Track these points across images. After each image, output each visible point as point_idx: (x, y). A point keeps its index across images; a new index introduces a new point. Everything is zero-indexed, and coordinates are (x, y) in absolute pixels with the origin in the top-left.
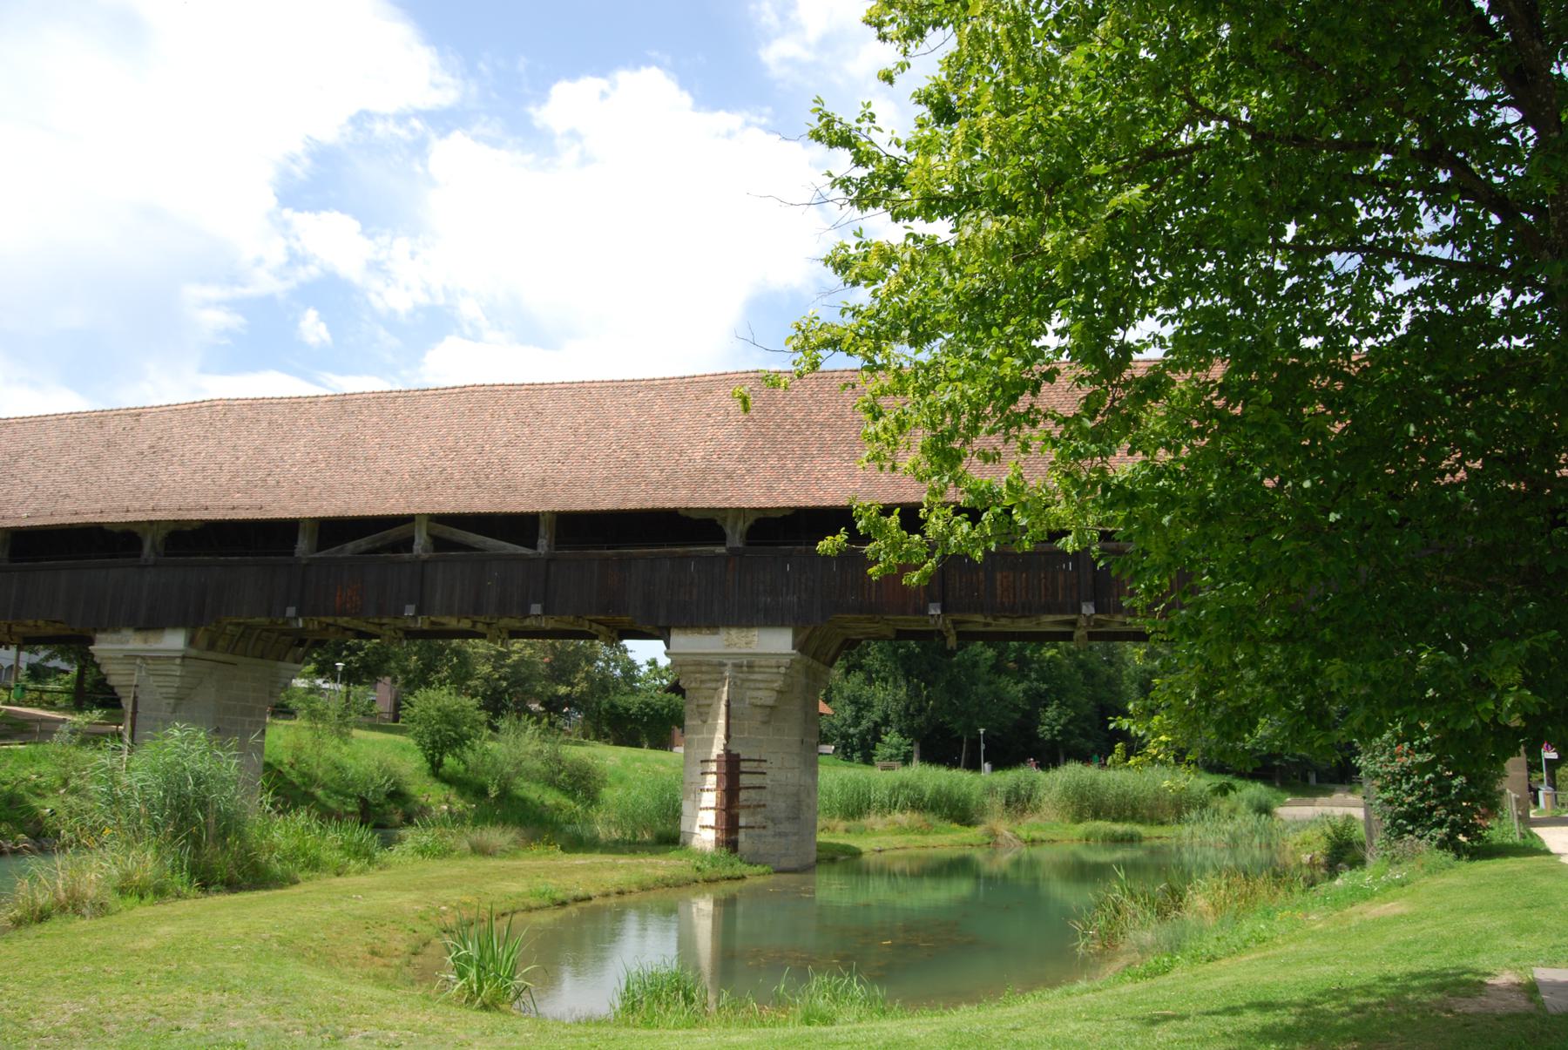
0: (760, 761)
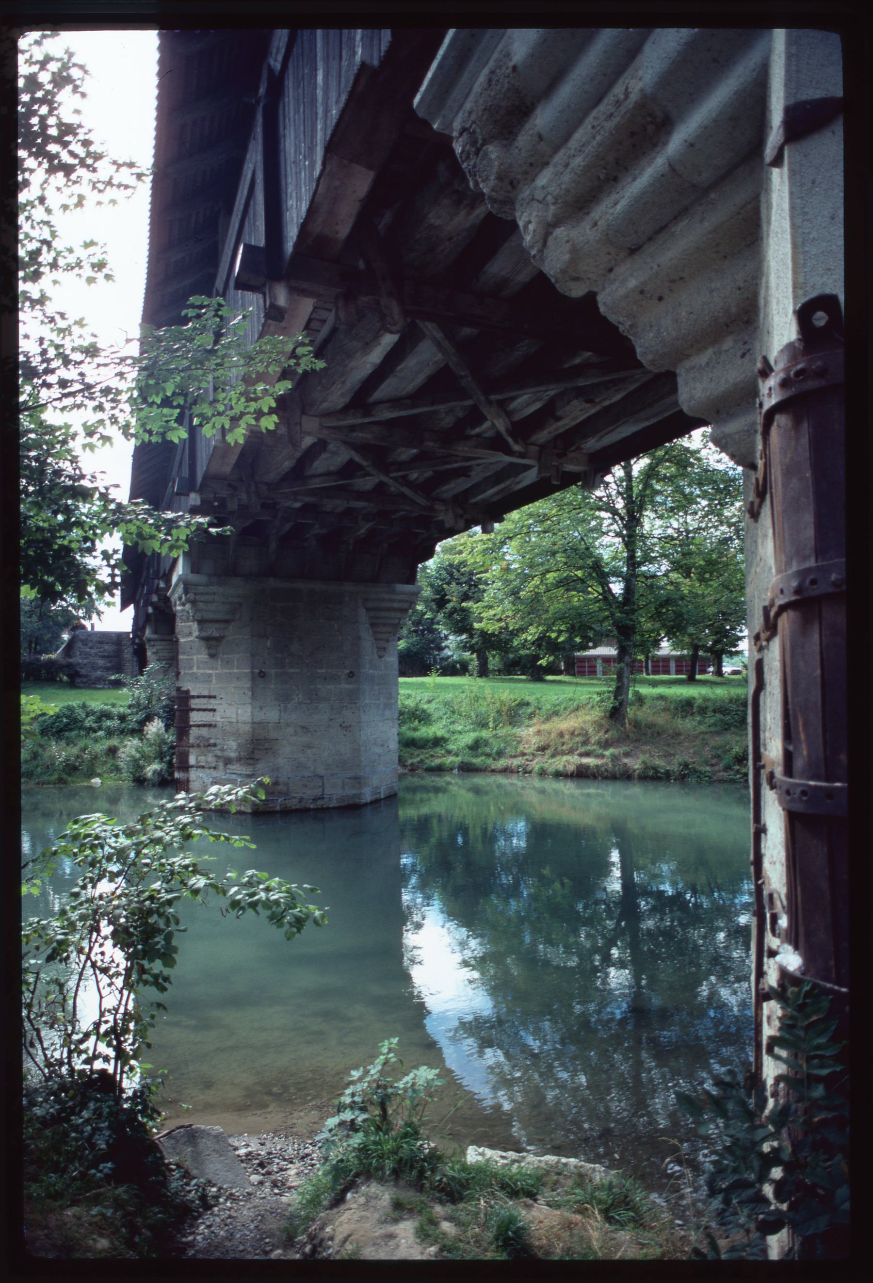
0: (210, 697)
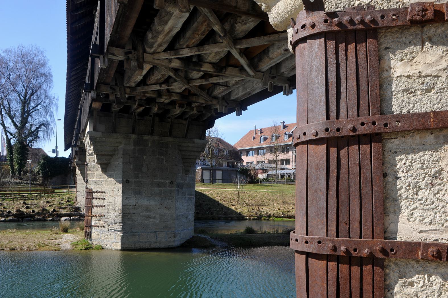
0: (102, 192)
